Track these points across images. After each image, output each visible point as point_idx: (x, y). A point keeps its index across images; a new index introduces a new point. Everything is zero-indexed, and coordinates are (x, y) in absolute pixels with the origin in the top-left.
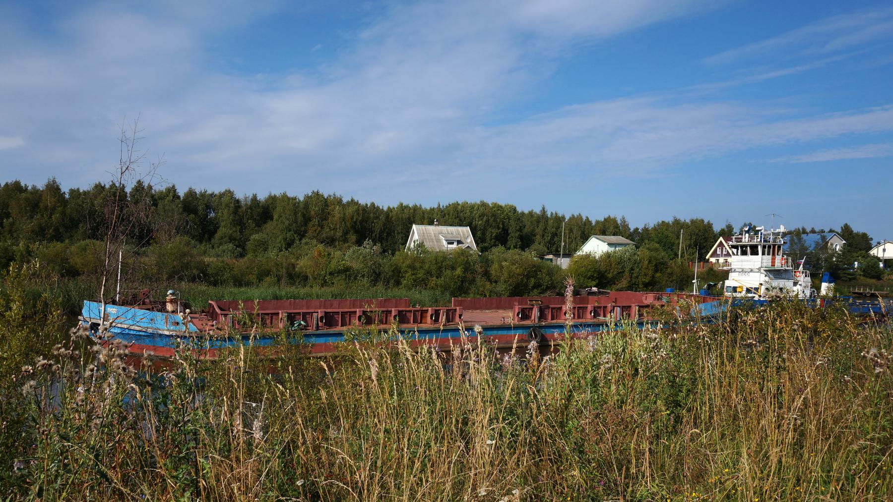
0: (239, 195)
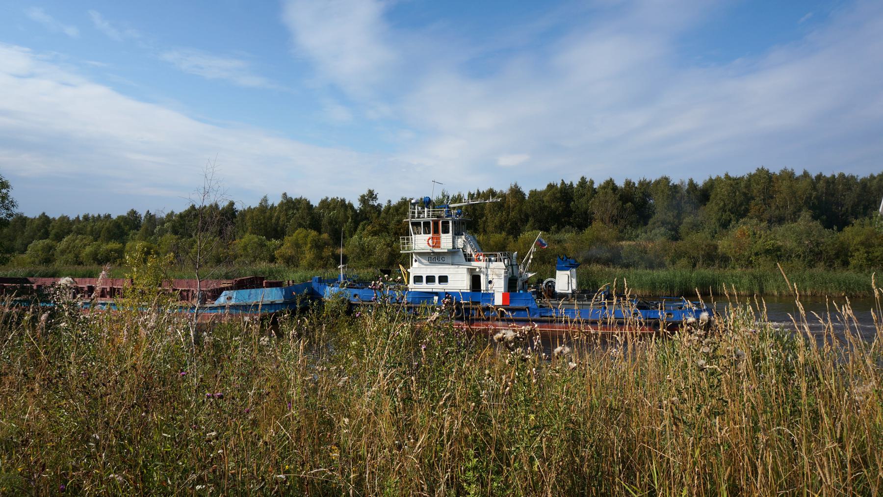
0: (675, 180)
